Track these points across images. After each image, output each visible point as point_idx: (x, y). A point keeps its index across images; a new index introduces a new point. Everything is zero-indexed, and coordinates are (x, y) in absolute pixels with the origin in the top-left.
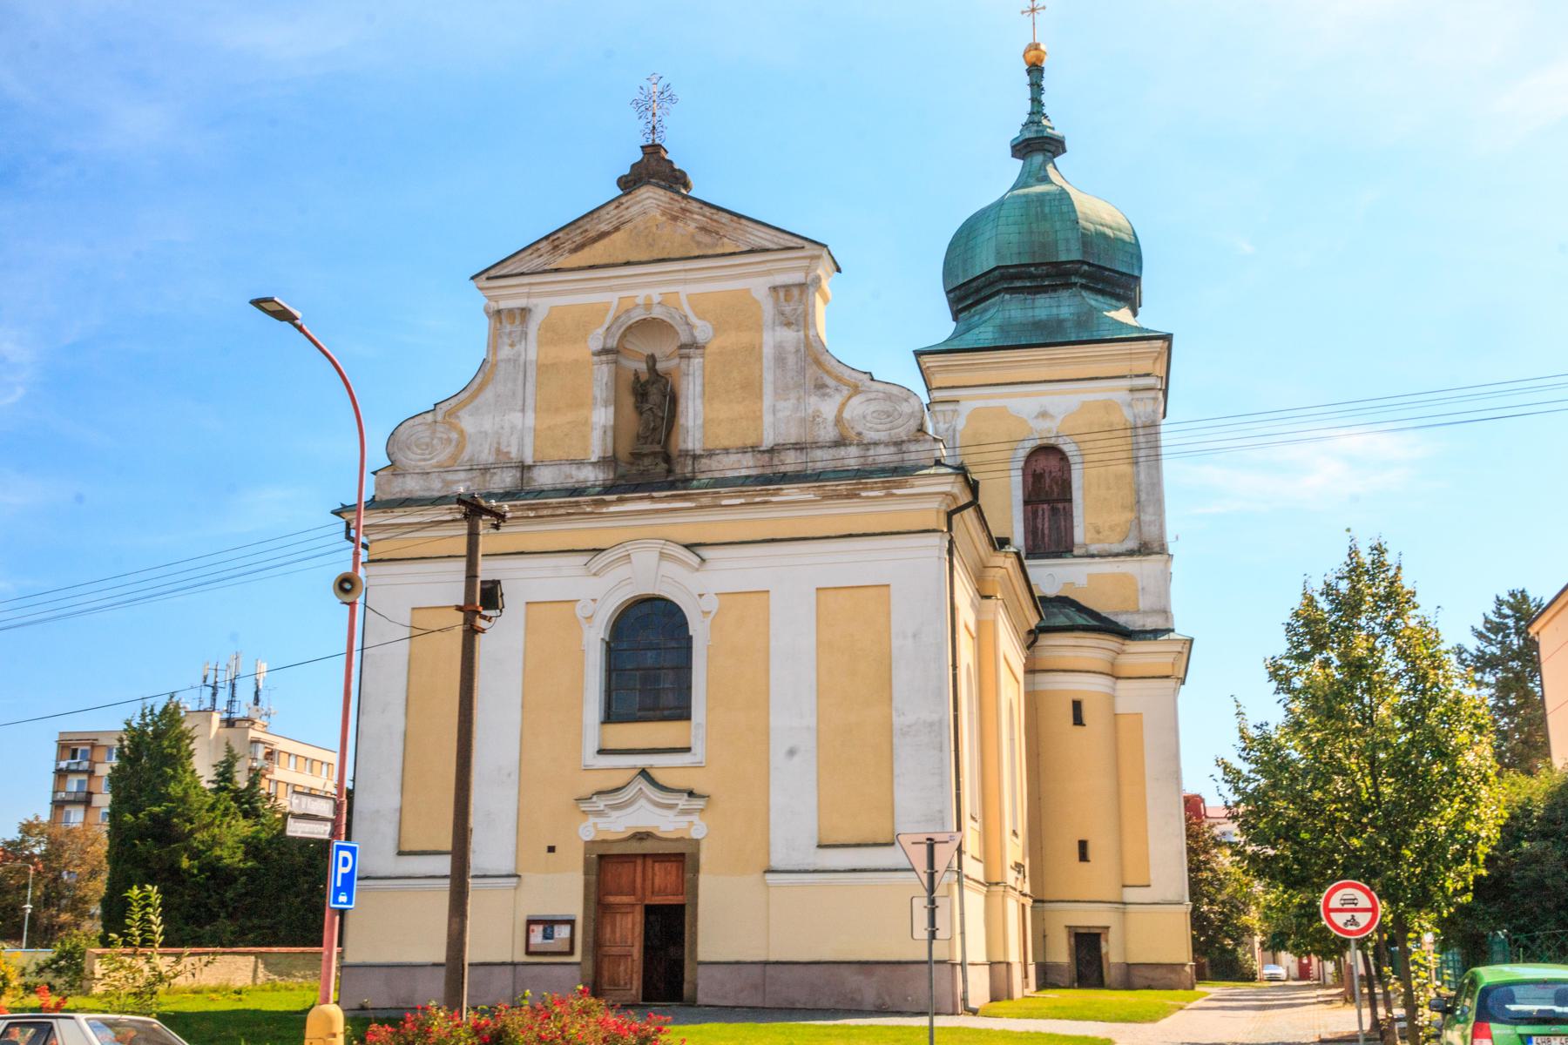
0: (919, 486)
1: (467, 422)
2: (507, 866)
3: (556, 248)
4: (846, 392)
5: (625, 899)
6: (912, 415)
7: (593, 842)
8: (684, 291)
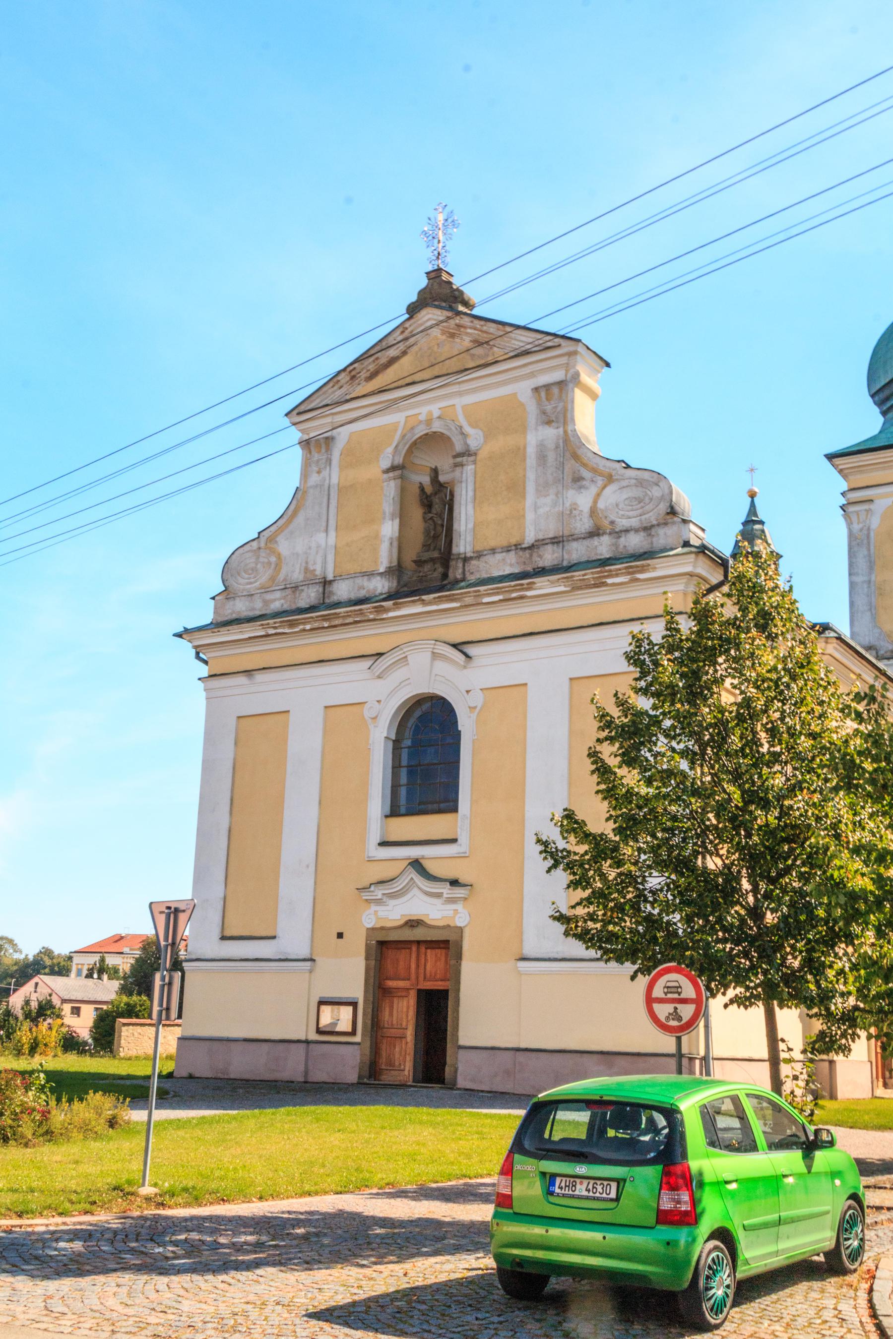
0: (661, 568)
1: (283, 546)
2: (305, 952)
3: (353, 378)
4: (600, 481)
5: (401, 984)
6: (662, 498)
7: (373, 929)
8: (459, 402)
